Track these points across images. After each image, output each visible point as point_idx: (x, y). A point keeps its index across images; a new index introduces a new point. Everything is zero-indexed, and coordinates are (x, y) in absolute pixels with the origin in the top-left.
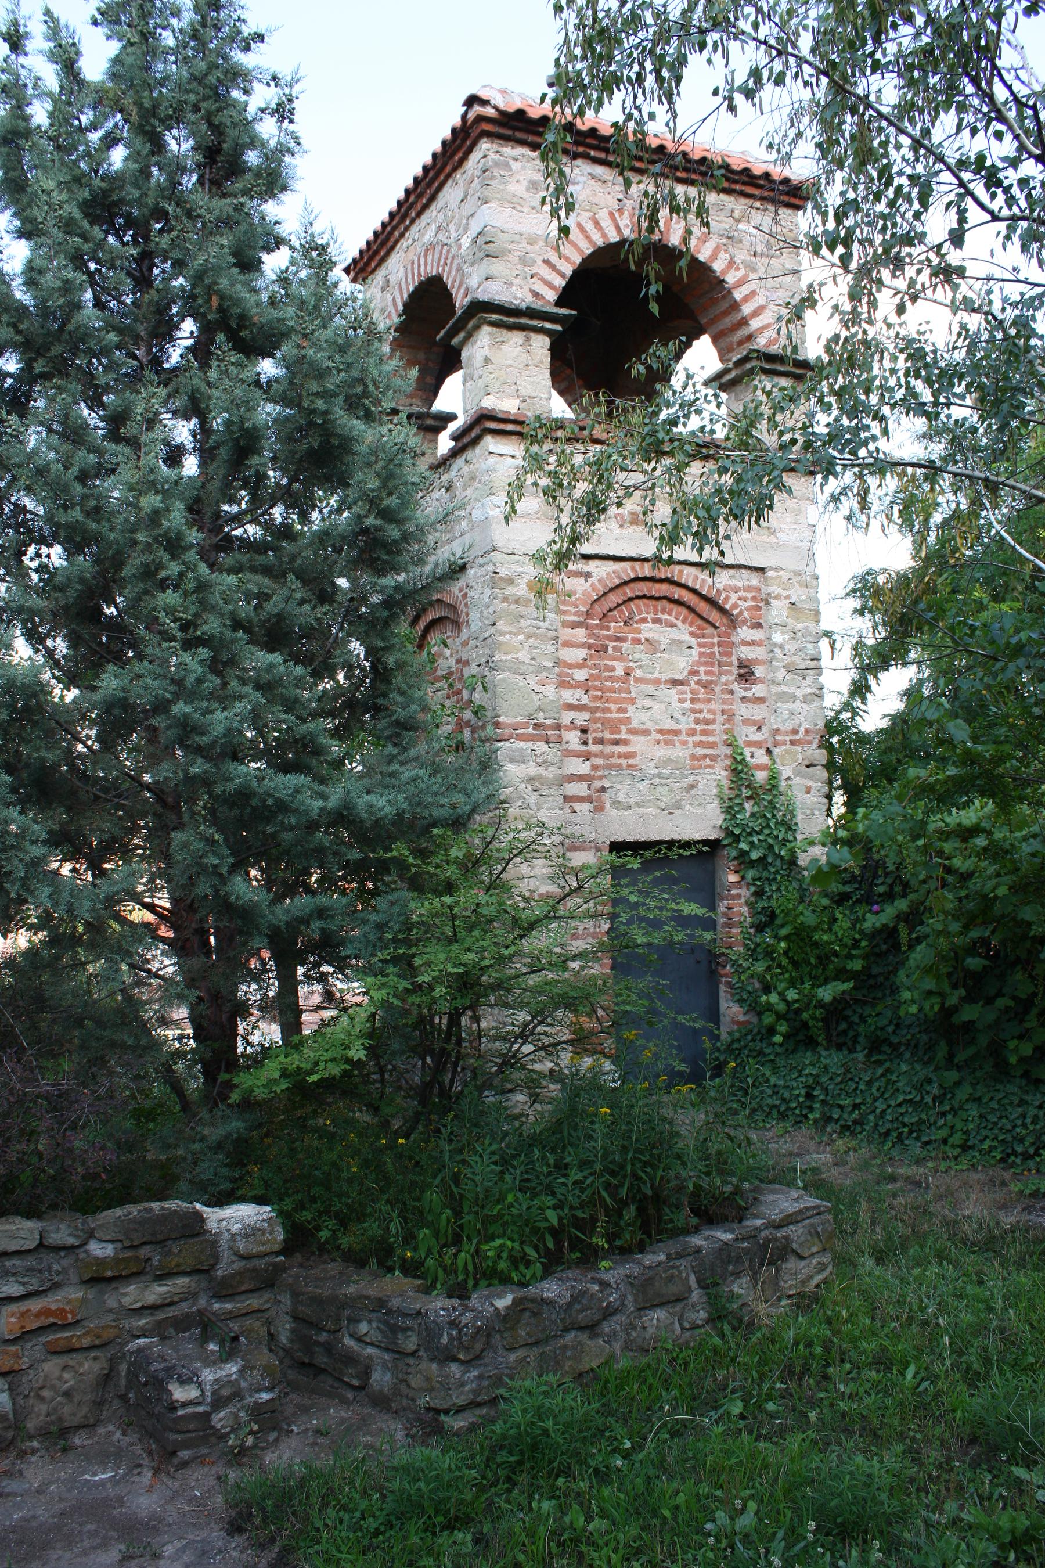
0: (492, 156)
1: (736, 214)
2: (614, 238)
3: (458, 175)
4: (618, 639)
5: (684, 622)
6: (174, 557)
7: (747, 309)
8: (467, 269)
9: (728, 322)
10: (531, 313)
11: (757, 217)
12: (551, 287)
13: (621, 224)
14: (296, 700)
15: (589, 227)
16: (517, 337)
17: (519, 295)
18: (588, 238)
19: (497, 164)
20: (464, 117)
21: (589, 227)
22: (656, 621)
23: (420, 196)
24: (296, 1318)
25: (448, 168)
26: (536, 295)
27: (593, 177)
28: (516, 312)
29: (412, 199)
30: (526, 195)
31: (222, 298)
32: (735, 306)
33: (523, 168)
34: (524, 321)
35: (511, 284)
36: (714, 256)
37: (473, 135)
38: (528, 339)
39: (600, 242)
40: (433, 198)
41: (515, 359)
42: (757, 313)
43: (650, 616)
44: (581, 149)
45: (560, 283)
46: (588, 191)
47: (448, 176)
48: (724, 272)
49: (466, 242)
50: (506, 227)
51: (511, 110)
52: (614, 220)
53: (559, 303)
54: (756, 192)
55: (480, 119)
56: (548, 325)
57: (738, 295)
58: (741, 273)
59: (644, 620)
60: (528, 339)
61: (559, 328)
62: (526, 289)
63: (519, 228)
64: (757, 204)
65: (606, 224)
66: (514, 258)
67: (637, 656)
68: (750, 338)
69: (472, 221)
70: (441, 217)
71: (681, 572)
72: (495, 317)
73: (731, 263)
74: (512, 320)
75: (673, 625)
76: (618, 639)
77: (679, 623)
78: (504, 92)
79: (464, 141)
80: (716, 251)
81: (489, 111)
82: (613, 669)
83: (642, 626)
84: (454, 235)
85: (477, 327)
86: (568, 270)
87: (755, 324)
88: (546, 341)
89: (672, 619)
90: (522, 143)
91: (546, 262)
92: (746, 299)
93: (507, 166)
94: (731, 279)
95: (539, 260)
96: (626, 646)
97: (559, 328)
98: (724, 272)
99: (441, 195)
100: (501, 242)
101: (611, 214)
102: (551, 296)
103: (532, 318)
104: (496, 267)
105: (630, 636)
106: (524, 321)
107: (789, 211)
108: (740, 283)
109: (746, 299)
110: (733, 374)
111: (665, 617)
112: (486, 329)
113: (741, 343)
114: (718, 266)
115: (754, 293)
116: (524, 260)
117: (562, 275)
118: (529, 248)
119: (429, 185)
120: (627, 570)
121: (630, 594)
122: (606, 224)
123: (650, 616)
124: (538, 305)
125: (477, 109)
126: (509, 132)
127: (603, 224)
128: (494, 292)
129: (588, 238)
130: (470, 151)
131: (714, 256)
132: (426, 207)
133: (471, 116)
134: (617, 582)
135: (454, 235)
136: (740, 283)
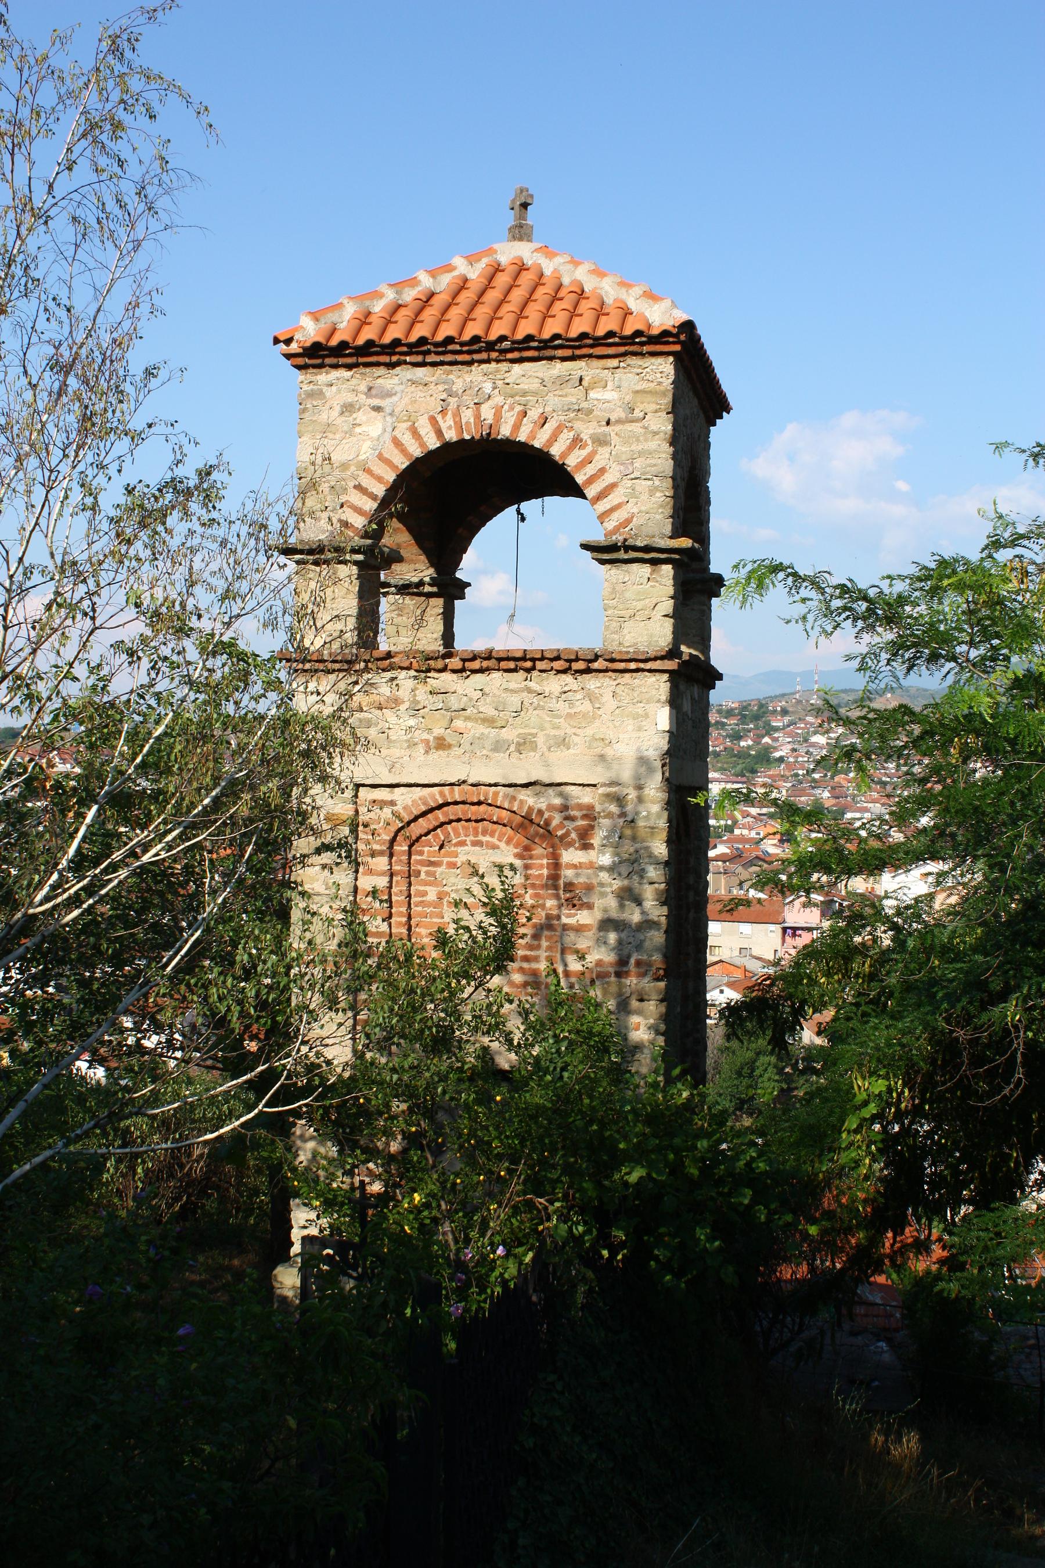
4: (431, 864)
5: (508, 843)
6: (841, 1100)
13: (444, 426)
14: (844, 725)
22: (475, 844)
24: (391, 285)
33: (339, 391)
39: (417, 452)
43: (469, 839)
44: (395, 358)
46: (406, 400)
54: (611, 351)
59: (462, 843)
64: (614, 362)
67: (453, 880)
71: (496, 794)
73: (577, 442)
75: (494, 847)
76: (431, 864)
77: (502, 845)
82: (425, 894)
83: (460, 849)
88: (355, 570)
89: (495, 840)
91: (358, 487)
93: (321, 393)
96: (439, 870)
101: (433, 420)
105: (446, 860)
108: (588, 460)
111: (487, 838)
115: (602, 471)
120: (435, 796)
121: (442, 819)
123: (469, 839)
134: (423, 808)
136: (588, 460)
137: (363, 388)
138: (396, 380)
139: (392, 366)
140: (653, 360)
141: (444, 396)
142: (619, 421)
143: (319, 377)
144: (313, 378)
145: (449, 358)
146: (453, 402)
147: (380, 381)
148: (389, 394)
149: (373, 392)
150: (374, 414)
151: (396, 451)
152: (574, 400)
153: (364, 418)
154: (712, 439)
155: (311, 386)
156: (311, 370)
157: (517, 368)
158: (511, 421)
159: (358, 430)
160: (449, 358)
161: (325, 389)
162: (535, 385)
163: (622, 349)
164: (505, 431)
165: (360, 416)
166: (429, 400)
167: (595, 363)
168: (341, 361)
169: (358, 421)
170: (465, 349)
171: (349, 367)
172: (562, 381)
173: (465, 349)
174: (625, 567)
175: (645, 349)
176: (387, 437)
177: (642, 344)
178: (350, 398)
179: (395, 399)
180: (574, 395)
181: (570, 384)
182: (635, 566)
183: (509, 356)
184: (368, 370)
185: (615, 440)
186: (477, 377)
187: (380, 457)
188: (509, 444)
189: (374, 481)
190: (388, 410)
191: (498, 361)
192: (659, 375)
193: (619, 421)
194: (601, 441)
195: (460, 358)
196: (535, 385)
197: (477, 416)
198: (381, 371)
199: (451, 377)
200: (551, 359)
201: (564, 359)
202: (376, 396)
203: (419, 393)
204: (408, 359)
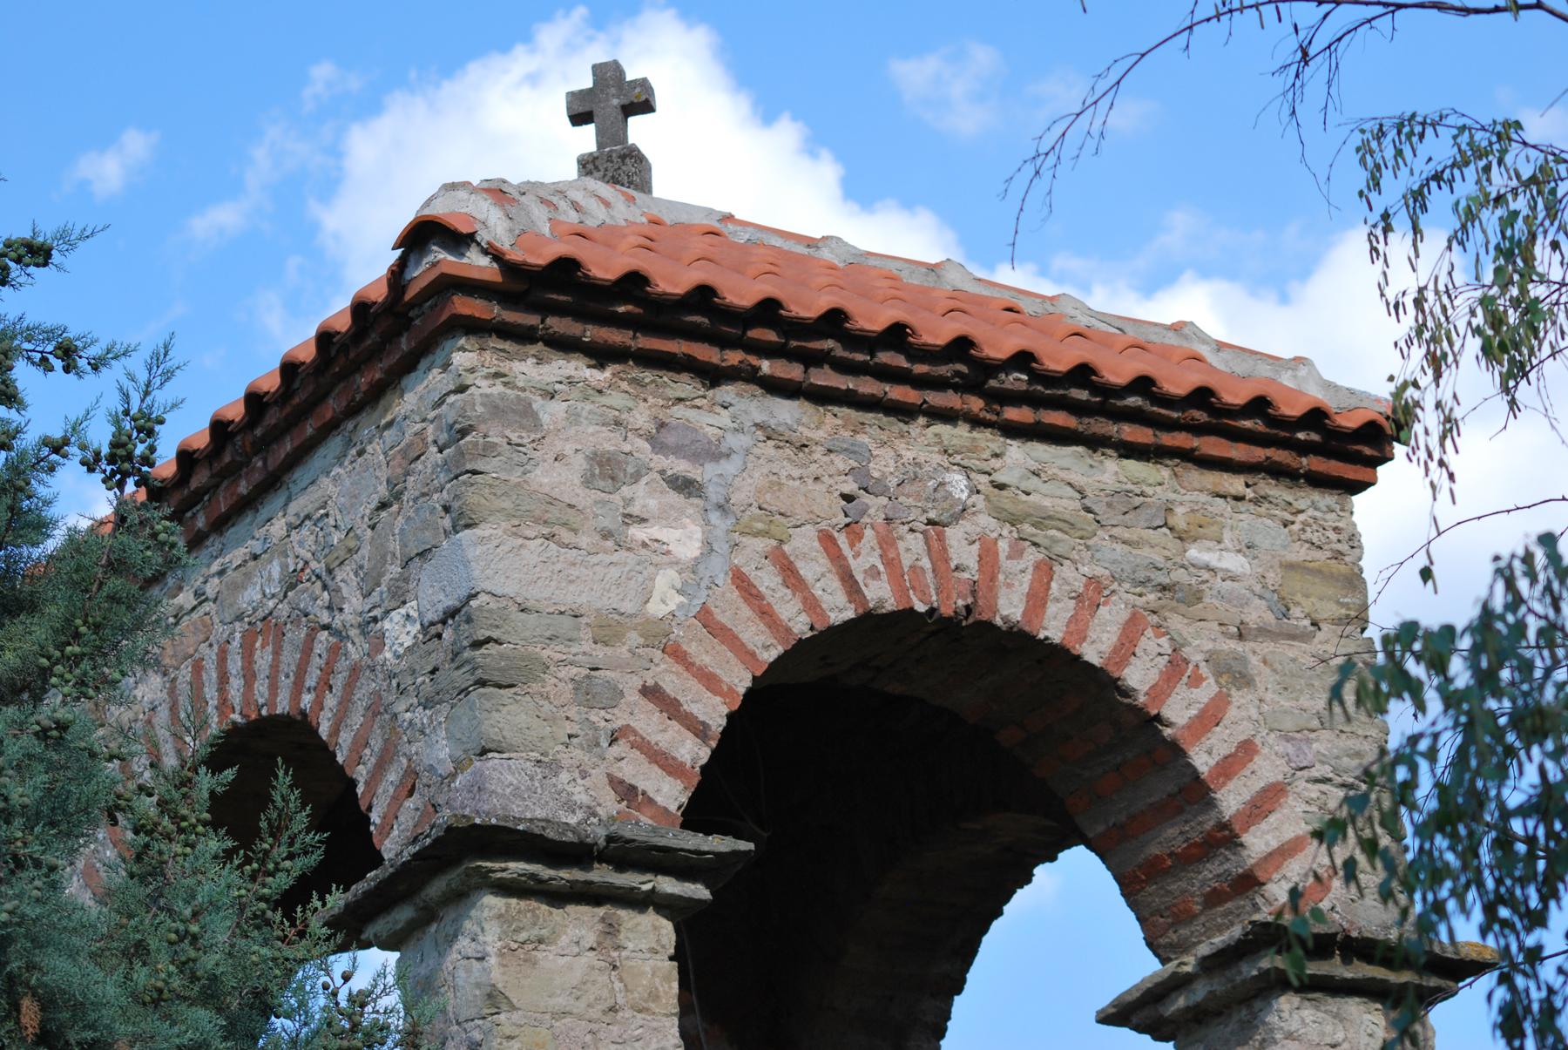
0: (483, 387)
1: (1179, 519)
2: (840, 610)
3: (365, 427)
7: (1231, 799)
8: (408, 712)
9: (1172, 836)
10: (624, 854)
11: (1245, 521)
12: (670, 766)
13: (858, 567)
15: (768, 581)
16: (580, 923)
17: (576, 799)
18: (766, 613)
19: (497, 410)
20: (397, 275)
21: (768, 581)
23: (231, 473)
25: (332, 407)
26: (627, 792)
27: (769, 433)
28: (577, 853)
29: (200, 479)
30: (585, 498)
31: (47, 1003)
32: (1197, 792)
33: (573, 417)
34: (601, 874)
35: (554, 767)
36: (1126, 647)
37: (422, 324)
38: (611, 928)
39: (801, 626)
40: (272, 483)
41: (577, 991)
42: (1265, 802)
44: (734, 357)
45: (694, 752)
46: (758, 476)
47: (329, 429)
48: (1161, 691)
49: (400, 631)
50: (533, 595)
51: (541, 258)
52: (836, 556)
53: (696, 816)
54: (1238, 452)
55: (450, 284)
56: (668, 885)
57: (1202, 760)
58: (1207, 691)
60: (611, 928)
61: (700, 892)
62: (598, 776)
63: (572, 597)
64: (1235, 484)
65: (816, 567)
66: (558, 684)
68: (1248, 883)
69: (425, 574)
70: (304, 543)
72: (516, 868)
73: (1176, 667)
74: (567, 874)
78: (498, 192)
79: (390, 338)
80: (1132, 631)
81: (476, 263)
84: (354, 604)
85: (460, 896)
86: (715, 713)
87: (1258, 842)
88: (665, 931)
90: (565, 345)
91: (652, 693)
92: (1229, 767)
93: (527, 415)
94: (1178, 711)
95: (631, 685)
97: (700, 892)
98: (1161, 691)
99: (300, 475)
100: (521, 638)
101: (827, 540)
102: (672, 794)
103: (621, 865)
104: (507, 716)
106: (601, 874)
107: (1327, 499)
108: (1210, 718)
109: (1229, 767)
110: (1200, 992)
112: (492, 903)
113: (1214, 899)
114: (1139, 676)
115: (1247, 749)
116: (591, 691)
117: (699, 730)
118: (600, 652)
119: (263, 446)
122: (816, 567)
124: (642, 828)
125: (440, 257)
126: (531, 320)
127: (807, 571)
128: (511, 792)
129: (766, 613)
130: (409, 365)
131: (1126, 647)
132: (247, 505)
133: (420, 274)
135: (354, 604)
136: (1210, 718)
137: (641, 417)
138: (724, 418)
139: (713, 376)
140: (1316, 495)
141: (850, 487)
142: (1264, 632)
143: (517, 366)
144: (505, 367)
145: (867, 386)
146: (875, 506)
147: (679, 411)
148: (715, 453)
149: (670, 439)
150: (674, 498)
151: (746, 611)
152: (1159, 560)
153: (652, 503)
154: (1074, 849)
155: (499, 388)
156: (494, 342)
157: (1019, 454)
158: (1024, 583)
159: (638, 533)
160: (867, 386)
161: (538, 403)
162: (1067, 504)
163: (1258, 454)
164: (1009, 607)
165: (646, 496)
166: (814, 493)
167: (1195, 476)
168: (591, 333)
169: (635, 510)
170: (920, 369)
171: (601, 356)
172: (1130, 502)
173: (920, 369)
174: (1334, 1004)
175: (1307, 463)
176: (718, 568)
177: (1304, 449)
178: (610, 442)
179: (729, 467)
180: (1157, 548)
181: (1144, 514)
182: (1354, 1007)
183: (1012, 414)
184: (648, 376)
185: (1265, 678)
186: (929, 458)
187: (705, 617)
188: (1018, 644)
189: (695, 685)
190: (714, 493)
191: (976, 422)
192: (1333, 536)
193: (1264, 632)
194: (1236, 675)
195: (897, 392)
196: (1067, 504)
197: (939, 554)
198: (685, 386)
199: (862, 438)
200: (1095, 443)
201: (1129, 451)
202: (678, 451)
203: (785, 465)
204: (766, 366)
